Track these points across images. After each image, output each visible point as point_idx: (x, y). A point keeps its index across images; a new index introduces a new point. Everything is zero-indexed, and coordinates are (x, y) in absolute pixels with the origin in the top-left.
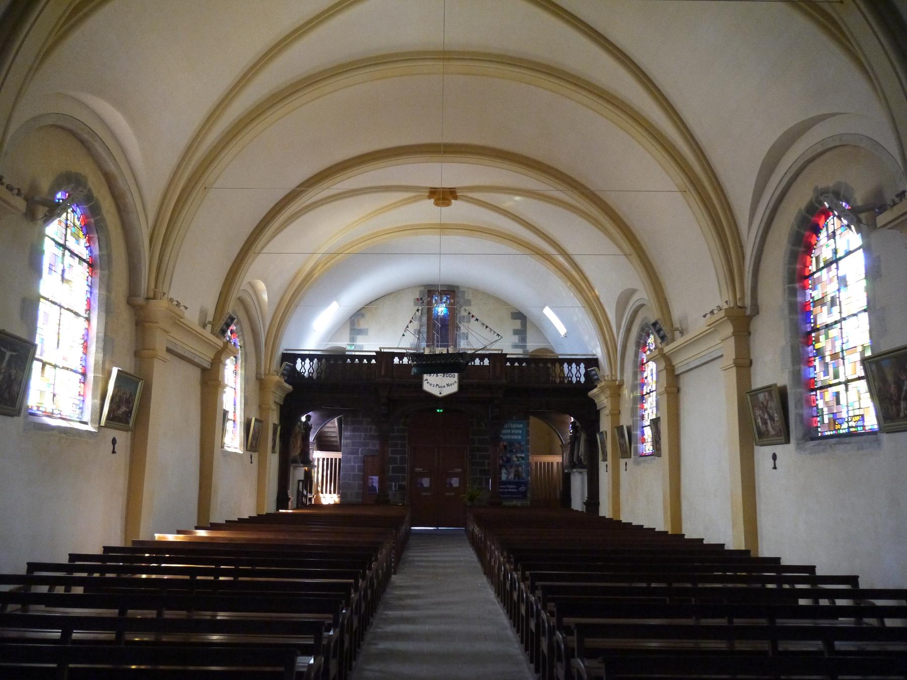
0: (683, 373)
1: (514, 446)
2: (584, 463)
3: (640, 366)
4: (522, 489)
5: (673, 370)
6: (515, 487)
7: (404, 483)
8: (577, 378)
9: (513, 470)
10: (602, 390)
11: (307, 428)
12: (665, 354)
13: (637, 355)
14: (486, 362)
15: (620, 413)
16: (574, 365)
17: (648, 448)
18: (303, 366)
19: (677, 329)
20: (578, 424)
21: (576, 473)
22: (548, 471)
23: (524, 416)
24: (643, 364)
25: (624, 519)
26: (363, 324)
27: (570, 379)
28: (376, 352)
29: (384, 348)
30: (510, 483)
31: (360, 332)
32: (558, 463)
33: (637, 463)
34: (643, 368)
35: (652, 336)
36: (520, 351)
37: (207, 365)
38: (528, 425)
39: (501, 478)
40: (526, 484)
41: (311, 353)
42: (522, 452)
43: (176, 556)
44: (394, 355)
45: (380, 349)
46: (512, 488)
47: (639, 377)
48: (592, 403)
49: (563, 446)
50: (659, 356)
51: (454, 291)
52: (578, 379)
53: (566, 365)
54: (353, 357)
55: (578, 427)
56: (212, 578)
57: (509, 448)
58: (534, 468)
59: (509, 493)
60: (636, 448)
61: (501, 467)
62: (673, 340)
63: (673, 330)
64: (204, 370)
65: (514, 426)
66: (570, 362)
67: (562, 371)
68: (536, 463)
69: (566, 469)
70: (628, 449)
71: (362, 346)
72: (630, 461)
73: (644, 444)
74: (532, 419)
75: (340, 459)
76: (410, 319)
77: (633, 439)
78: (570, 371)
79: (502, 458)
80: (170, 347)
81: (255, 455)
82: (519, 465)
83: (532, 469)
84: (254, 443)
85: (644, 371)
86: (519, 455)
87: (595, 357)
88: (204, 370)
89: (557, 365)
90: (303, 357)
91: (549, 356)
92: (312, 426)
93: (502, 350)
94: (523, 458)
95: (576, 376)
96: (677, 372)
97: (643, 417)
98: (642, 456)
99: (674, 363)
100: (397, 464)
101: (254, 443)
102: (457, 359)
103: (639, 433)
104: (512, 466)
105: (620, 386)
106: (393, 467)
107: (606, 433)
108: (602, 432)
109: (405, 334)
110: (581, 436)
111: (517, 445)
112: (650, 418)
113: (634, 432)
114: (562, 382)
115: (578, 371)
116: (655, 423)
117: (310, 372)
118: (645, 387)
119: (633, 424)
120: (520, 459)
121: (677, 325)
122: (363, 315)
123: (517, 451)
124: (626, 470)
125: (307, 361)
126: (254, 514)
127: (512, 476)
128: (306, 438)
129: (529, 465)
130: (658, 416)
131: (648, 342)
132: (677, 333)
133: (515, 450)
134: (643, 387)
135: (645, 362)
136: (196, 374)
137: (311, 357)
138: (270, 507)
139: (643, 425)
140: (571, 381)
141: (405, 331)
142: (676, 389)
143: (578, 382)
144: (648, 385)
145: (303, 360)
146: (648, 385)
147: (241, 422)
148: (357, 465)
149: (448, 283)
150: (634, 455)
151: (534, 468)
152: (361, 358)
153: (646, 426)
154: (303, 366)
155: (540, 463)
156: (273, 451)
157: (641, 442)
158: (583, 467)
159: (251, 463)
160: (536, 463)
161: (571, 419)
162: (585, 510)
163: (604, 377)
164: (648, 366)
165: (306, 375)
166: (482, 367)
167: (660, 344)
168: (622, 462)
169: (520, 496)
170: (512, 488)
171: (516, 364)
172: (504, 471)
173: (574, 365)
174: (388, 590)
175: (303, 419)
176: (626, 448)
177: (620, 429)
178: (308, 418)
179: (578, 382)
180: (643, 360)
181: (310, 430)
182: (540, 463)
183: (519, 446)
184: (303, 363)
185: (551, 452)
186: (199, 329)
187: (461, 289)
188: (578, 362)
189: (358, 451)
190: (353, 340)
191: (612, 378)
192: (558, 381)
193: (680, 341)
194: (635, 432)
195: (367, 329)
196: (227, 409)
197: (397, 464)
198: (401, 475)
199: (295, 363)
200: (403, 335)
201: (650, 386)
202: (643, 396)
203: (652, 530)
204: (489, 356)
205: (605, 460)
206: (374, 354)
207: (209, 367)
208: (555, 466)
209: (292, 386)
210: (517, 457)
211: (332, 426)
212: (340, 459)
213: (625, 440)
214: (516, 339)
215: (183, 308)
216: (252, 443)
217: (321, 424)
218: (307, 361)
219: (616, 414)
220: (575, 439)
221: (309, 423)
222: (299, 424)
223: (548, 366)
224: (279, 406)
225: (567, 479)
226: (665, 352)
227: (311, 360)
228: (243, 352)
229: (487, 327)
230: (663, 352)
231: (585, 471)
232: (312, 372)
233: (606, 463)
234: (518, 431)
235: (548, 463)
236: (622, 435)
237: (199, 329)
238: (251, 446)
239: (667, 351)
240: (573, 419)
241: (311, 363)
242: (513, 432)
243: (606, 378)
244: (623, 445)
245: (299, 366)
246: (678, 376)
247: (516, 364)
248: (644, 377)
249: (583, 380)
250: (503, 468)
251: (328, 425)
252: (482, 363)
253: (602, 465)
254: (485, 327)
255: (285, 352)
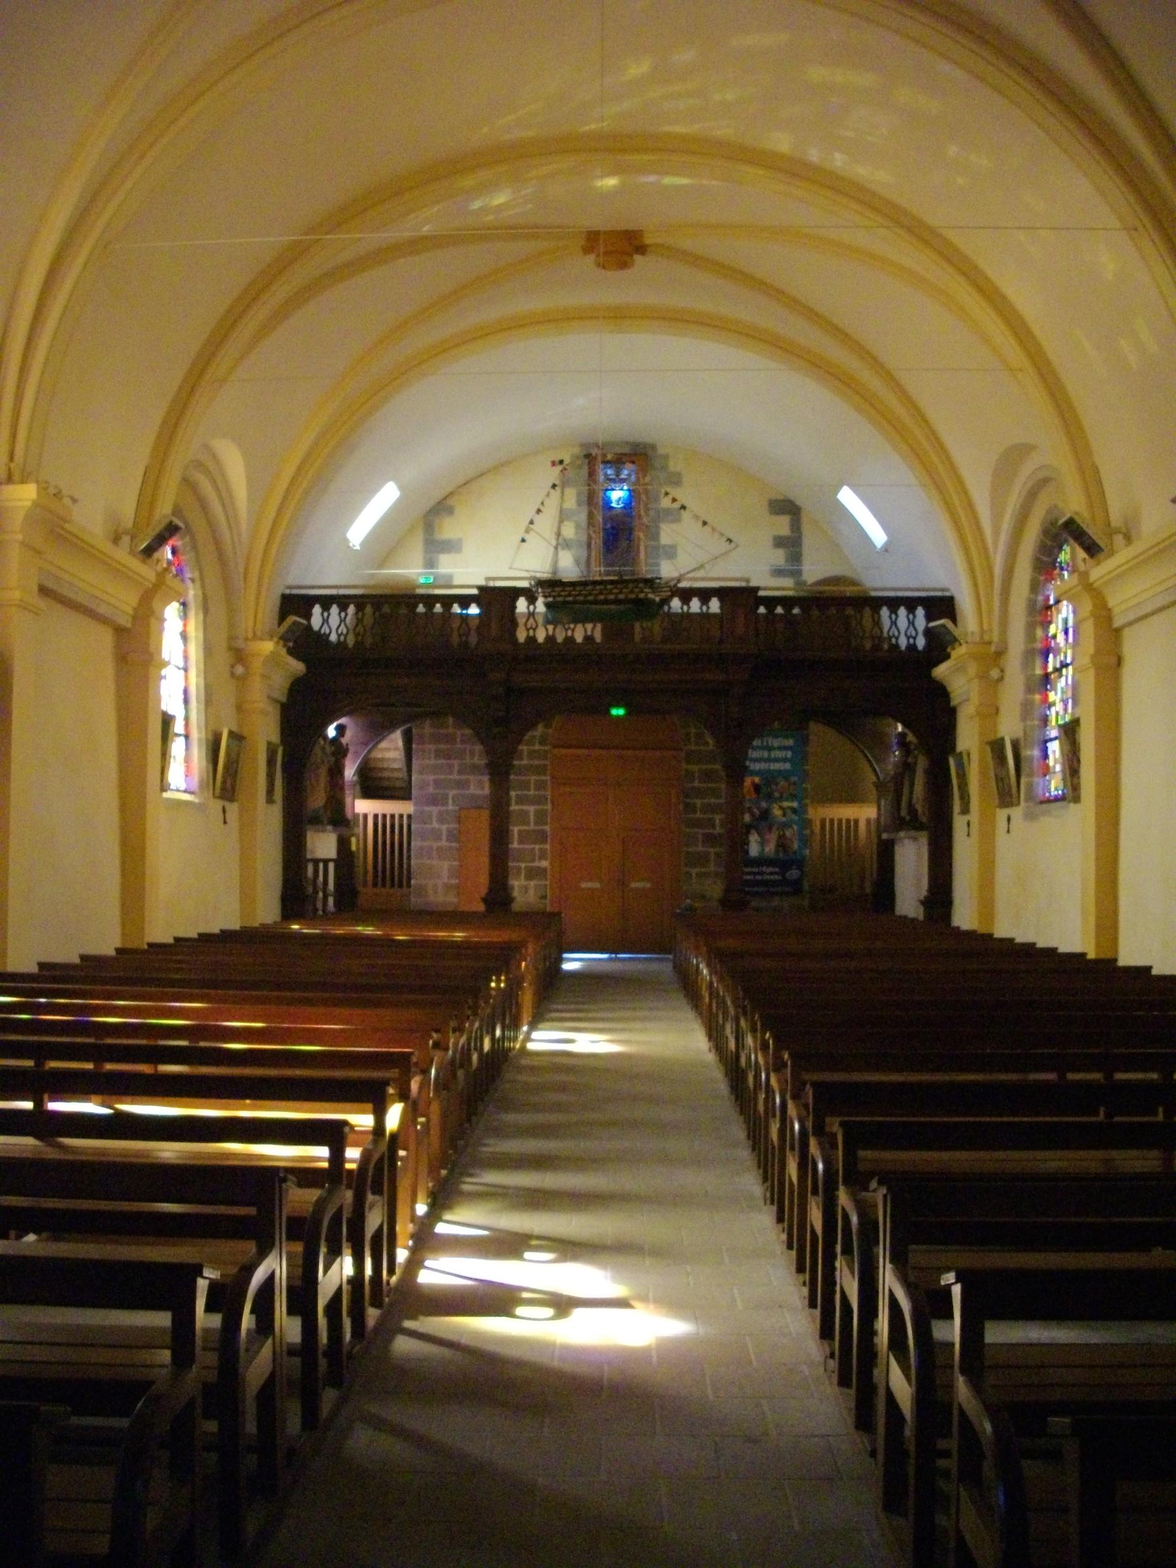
0: (1130, 624)
1: (776, 784)
2: (924, 820)
3: (1042, 613)
4: (793, 874)
5: (1109, 619)
6: (777, 870)
7: (545, 864)
8: (908, 638)
9: (772, 838)
10: (961, 669)
11: (339, 750)
12: (1091, 584)
13: (1035, 587)
14: (715, 605)
15: (997, 709)
16: (902, 611)
17: (1055, 786)
18: (325, 621)
19: (1117, 531)
20: (911, 737)
21: (906, 841)
22: (848, 838)
23: (797, 724)
24: (1049, 607)
25: (1002, 930)
26: (448, 529)
27: (894, 641)
28: (481, 588)
29: (494, 579)
30: (769, 862)
31: (450, 547)
32: (868, 821)
33: (1030, 816)
34: (1046, 616)
35: (1067, 548)
36: (788, 582)
37: (125, 621)
38: (805, 741)
39: (747, 852)
40: (800, 863)
41: (342, 592)
42: (793, 797)
43: (34, 1017)
44: (515, 593)
45: (488, 579)
46: (770, 874)
47: (1039, 633)
48: (941, 692)
49: (879, 786)
50: (1080, 588)
51: (646, 455)
52: (911, 641)
53: (885, 612)
54: (430, 600)
55: (910, 742)
56: (30, 1063)
57: (764, 790)
58: (817, 829)
59: (766, 883)
60: (1030, 786)
61: (748, 828)
62: (1112, 553)
63: (1111, 532)
64: (119, 631)
65: (776, 743)
66: (894, 603)
67: (877, 623)
68: (823, 821)
69: (884, 831)
70: (1014, 790)
71: (450, 577)
72: (1017, 813)
73: (1047, 777)
74: (816, 729)
75: (409, 817)
76: (537, 505)
77: (1024, 765)
78: (894, 623)
79: (750, 810)
80: (50, 584)
81: (233, 809)
82: (785, 825)
83: (812, 832)
84: (229, 782)
85: (1050, 622)
86: (786, 804)
87: (947, 594)
88: (119, 631)
89: (867, 611)
90: (326, 602)
91: (849, 591)
92: (350, 747)
93: (748, 581)
94: (794, 811)
95: (906, 635)
96: (1117, 623)
97: (1045, 720)
98: (1042, 802)
99: (1110, 605)
100: (528, 824)
101: (229, 782)
102: (642, 592)
103: (1036, 753)
104: (770, 829)
105: (1000, 654)
106: (520, 832)
107: (969, 755)
108: (961, 753)
109: (527, 537)
110: (915, 763)
111: (782, 783)
112: (1061, 722)
113: (1025, 753)
114: (876, 648)
115: (912, 623)
116: (1070, 731)
117: (340, 631)
118: (1051, 656)
119: (1025, 734)
120: (789, 812)
121: (1115, 519)
122: (450, 511)
123: (781, 796)
124: (1008, 831)
125: (334, 609)
126: (235, 925)
127: (770, 848)
128: (337, 771)
129: (807, 823)
130: (1076, 716)
131: (1059, 560)
132: (1119, 540)
133: (777, 794)
134: (1047, 657)
135: (1052, 602)
136: (105, 638)
137: (342, 602)
138: (267, 911)
139: (1048, 738)
140: (897, 646)
141: (527, 531)
142: (1113, 660)
143: (912, 648)
144: (1057, 652)
145: (326, 607)
146: (1057, 652)
147: (200, 740)
148: (444, 827)
149: (631, 439)
150: (1026, 801)
151: (817, 829)
152: (448, 601)
153: (1051, 740)
154: (325, 621)
155: (832, 821)
156: (270, 800)
157: (1041, 772)
158: (920, 827)
159: (225, 822)
160: (823, 821)
161: (896, 728)
162: (921, 917)
163: (966, 634)
164: (1059, 612)
165: (333, 638)
166: (706, 616)
167: (1082, 564)
168: (1002, 814)
169: (787, 889)
170: (771, 873)
171: (779, 610)
172: (754, 838)
173: (902, 611)
174: (508, 1076)
175: (331, 732)
176: (1009, 786)
177: (997, 747)
178: (341, 729)
179: (912, 648)
180: (1048, 599)
181: (345, 755)
182: (832, 821)
183: (786, 784)
184: (326, 614)
185: (853, 797)
186: (106, 546)
187: (661, 451)
188: (911, 604)
189: (447, 798)
190: (430, 564)
191: (982, 638)
192: (868, 645)
193: (1122, 556)
194: (1029, 753)
195: (460, 540)
196: (170, 712)
197: (528, 824)
198: (537, 847)
199: (308, 616)
200: (523, 540)
201: (1062, 655)
202: (1047, 676)
203: (1051, 952)
204: (721, 593)
205: (965, 810)
206: (475, 591)
207: (129, 625)
208: (862, 826)
209: (304, 661)
210: (781, 808)
211: (391, 749)
212: (409, 817)
213: (1008, 769)
214: (779, 557)
215: (67, 501)
216: (224, 782)
217: (366, 744)
218: (334, 609)
219: (991, 712)
220: (907, 768)
221: (344, 741)
222: (322, 742)
223: (847, 613)
224: (279, 706)
225: (886, 853)
226: (1091, 580)
227: (343, 608)
228: (200, 593)
229: (705, 523)
230: (1088, 579)
231: (924, 839)
232: (345, 632)
233: (966, 818)
234: (784, 753)
235: (848, 821)
236: (1000, 758)
237: (106, 546)
238: (223, 789)
239: (1095, 579)
240: (900, 728)
241: (343, 614)
242: (773, 756)
243: (969, 639)
244: (1002, 779)
245: (316, 621)
246: (1118, 631)
247: (779, 610)
248: (1050, 635)
249: (921, 643)
250: (753, 831)
251: (383, 745)
252: (704, 608)
253: (959, 823)
254: (700, 523)
255: (288, 592)
